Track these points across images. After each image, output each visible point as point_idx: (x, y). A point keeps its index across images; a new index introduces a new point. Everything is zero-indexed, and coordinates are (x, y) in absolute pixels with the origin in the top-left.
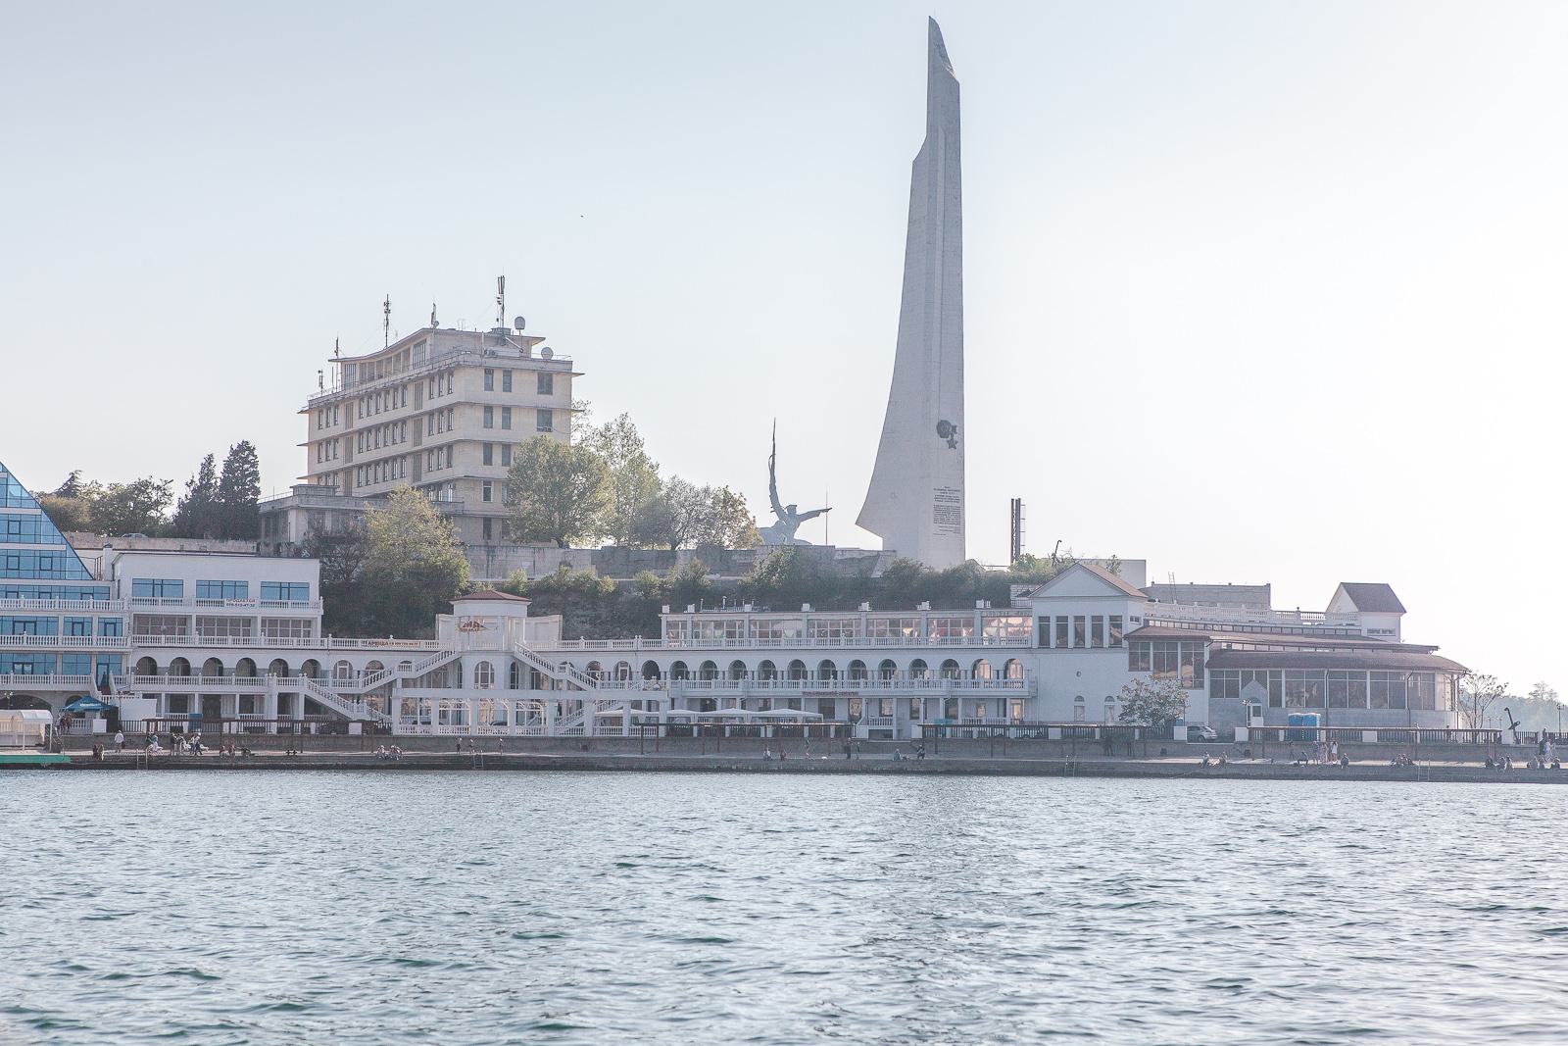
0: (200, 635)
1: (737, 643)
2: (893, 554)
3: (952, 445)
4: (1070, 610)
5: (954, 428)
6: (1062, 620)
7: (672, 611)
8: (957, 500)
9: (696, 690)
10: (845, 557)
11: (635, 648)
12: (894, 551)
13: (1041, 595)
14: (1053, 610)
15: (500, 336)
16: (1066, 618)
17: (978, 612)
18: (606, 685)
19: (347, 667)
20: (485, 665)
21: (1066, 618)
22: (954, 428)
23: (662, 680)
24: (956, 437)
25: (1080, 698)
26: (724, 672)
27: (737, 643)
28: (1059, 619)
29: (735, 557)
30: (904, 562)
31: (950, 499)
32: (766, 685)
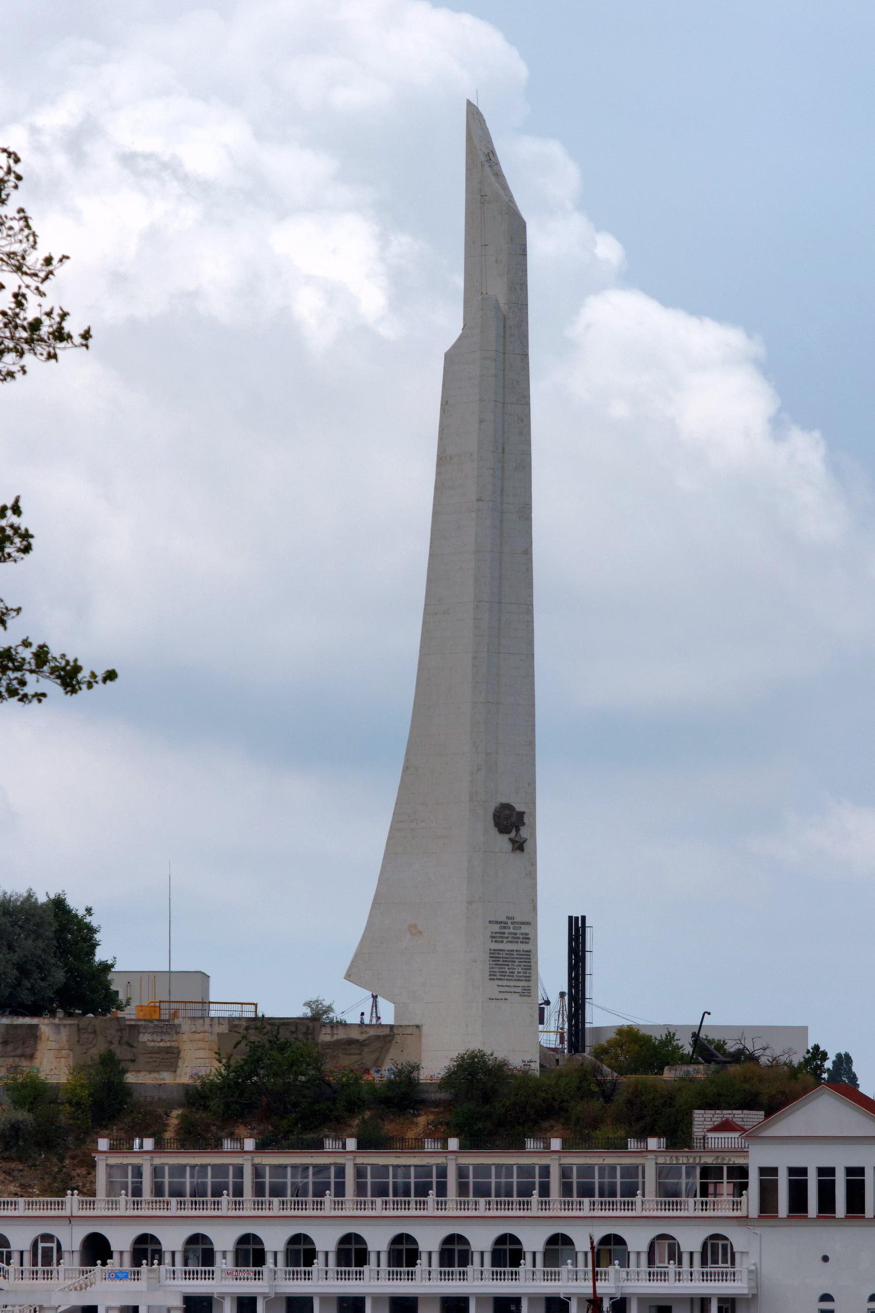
0: (126, 1195)
1: (413, 1205)
2: (415, 1031)
3: (519, 846)
4: (812, 1160)
5: (521, 814)
6: (798, 1174)
7: (114, 1149)
8: (526, 939)
9: (431, 1283)
10: (335, 1038)
11: (67, 1213)
12: (418, 1027)
13: (763, 1135)
14: (783, 1159)
16: (803, 1171)
17: (651, 1156)
18: (685, 1276)
19: (54, 1245)
21: (803, 1171)
22: (521, 814)
23: (633, 1268)
24: (524, 832)
25: (826, 1298)
26: (173, 1253)
27: (413, 1205)
28: (792, 1171)
29: (144, 1038)
30: (476, 1056)
31: (515, 939)
32: (556, 1276)
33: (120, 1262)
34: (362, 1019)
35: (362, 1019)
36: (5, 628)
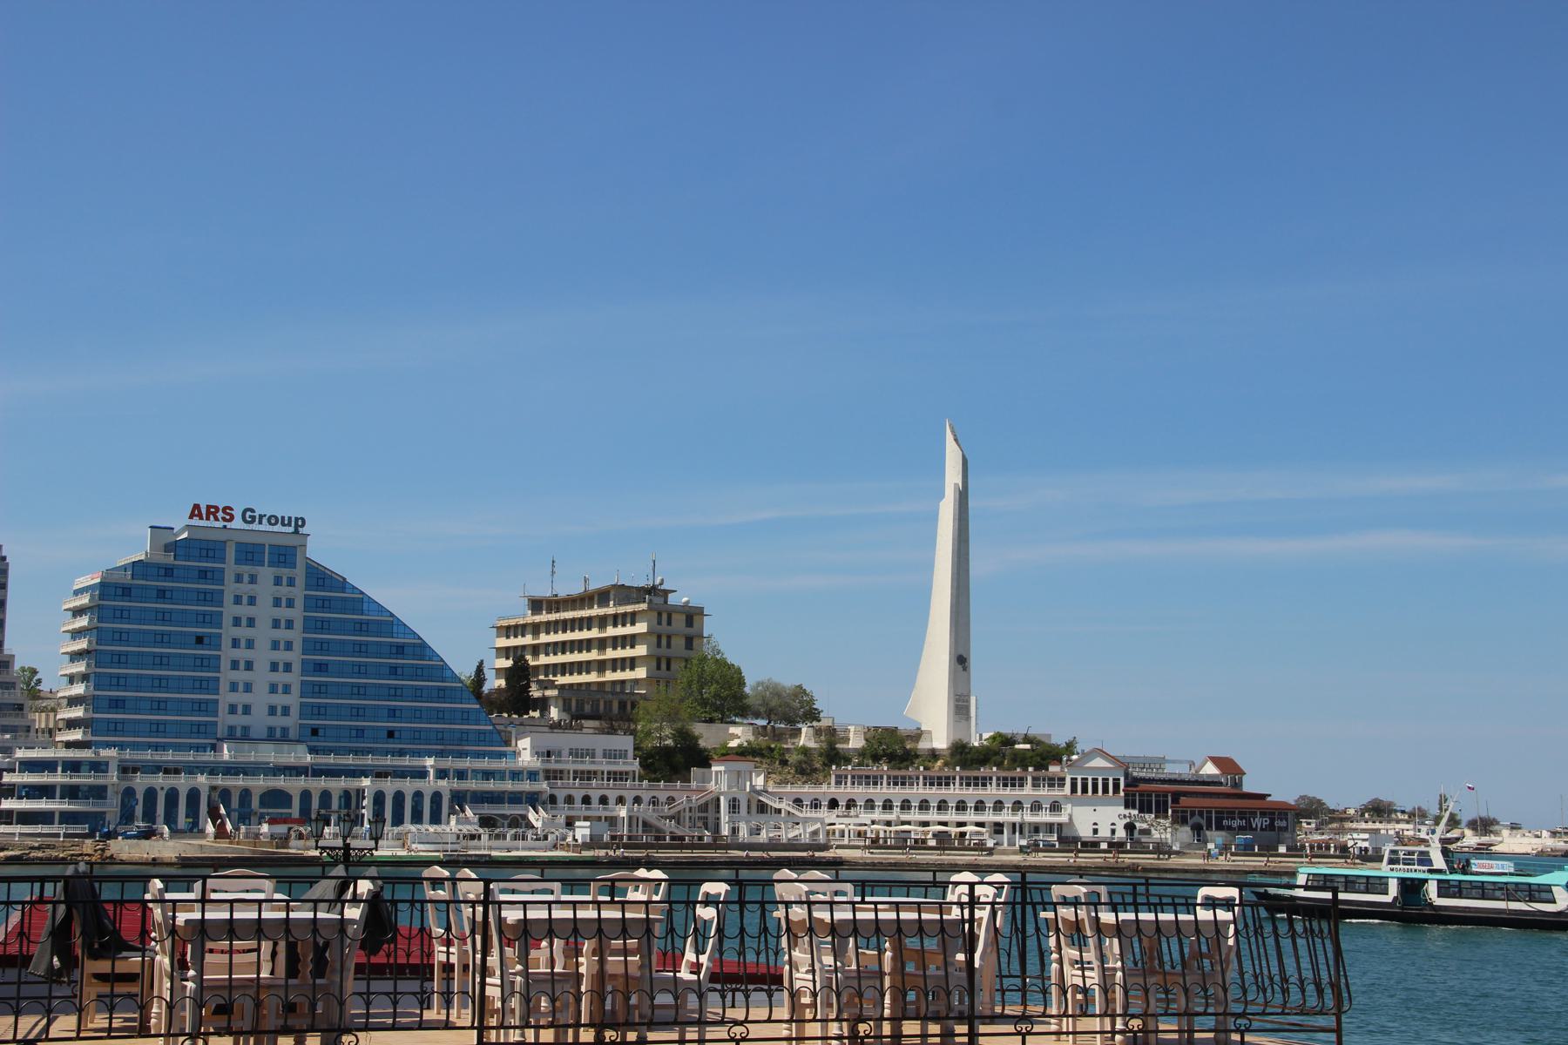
3: (965, 669)
15: (652, 590)
20: (734, 799)
33: (896, 810)
34: (1095, 831)
35: (1095, 831)
36: (481, 663)
